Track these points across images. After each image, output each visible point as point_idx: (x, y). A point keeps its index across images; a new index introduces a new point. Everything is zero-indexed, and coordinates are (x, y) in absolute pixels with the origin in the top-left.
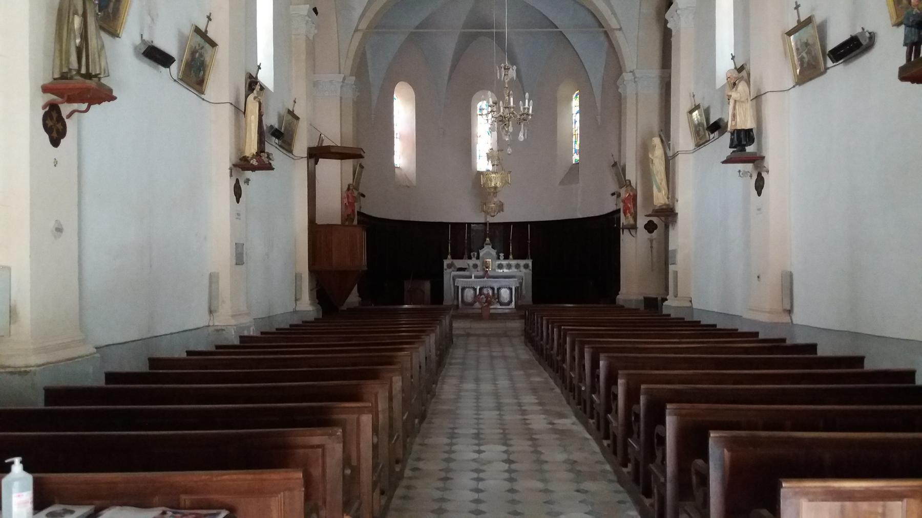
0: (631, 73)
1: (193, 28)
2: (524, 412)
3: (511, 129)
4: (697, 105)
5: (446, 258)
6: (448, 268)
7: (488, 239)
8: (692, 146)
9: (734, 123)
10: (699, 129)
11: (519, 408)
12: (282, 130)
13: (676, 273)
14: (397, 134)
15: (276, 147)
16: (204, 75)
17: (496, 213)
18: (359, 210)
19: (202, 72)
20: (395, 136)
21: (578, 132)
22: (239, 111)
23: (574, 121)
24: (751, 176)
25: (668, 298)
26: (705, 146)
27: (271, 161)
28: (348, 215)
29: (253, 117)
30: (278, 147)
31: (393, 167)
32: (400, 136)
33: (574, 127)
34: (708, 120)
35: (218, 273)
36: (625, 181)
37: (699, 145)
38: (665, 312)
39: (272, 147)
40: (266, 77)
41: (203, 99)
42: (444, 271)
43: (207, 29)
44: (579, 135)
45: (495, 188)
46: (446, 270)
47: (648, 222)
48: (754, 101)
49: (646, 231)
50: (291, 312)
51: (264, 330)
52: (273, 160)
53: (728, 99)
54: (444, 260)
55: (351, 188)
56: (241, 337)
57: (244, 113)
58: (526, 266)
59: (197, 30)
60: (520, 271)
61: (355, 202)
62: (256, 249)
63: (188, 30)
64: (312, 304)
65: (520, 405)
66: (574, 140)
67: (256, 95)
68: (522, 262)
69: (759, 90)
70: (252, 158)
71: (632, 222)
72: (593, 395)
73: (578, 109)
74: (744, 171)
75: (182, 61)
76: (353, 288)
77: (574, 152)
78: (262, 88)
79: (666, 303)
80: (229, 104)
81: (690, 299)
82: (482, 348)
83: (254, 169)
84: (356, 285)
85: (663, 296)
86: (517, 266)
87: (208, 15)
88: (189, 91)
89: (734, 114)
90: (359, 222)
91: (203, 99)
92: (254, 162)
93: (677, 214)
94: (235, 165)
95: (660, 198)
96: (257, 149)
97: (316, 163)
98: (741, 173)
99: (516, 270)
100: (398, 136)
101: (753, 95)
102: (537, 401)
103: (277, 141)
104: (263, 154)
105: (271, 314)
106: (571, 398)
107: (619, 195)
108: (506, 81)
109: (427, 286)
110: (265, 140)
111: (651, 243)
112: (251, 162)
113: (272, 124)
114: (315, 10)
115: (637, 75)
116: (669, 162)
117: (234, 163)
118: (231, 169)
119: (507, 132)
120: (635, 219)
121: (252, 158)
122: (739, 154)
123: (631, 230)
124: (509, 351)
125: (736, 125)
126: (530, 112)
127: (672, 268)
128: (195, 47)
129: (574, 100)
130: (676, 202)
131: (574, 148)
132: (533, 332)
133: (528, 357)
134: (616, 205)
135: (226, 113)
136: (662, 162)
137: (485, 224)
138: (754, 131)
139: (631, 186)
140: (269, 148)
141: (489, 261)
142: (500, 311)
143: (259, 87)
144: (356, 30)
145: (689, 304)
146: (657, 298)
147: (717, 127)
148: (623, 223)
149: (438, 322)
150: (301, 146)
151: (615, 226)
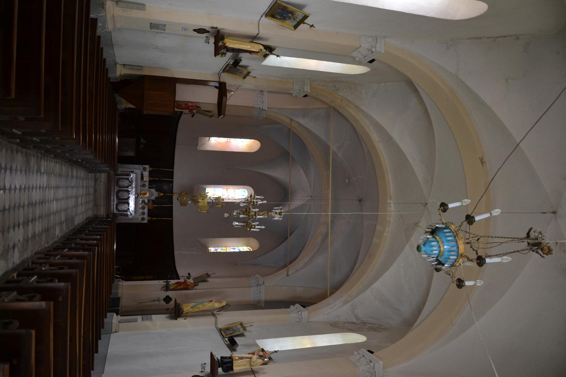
0: (262, 283)
1: (308, 15)
2: (26, 223)
3: (241, 216)
4: (246, 328)
5: (150, 167)
6: (143, 168)
7: (162, 194)
8: (220, 326)
9: (237, 358)
10: (231, 330)
11: (30, 219)
12: (238, 67)
13: (136, 321)
14: (230, 140)
15: (227, 62)
16: (277, 18)
17: (180, 201)
18: (184, 112)
19: (279, 17)
20: (229, 139)
21: (228, 251)
22: (253, 39)
23: (234, 248)
24: (202, 372)
25: (119, 316)
26: (220, 335)
27: (220, 55)
28: (180, 105)
29: (249, 47)
30: (227, 63)
32: (229, 142)
33: (231, 248)
34: (237, 336)
35: (145, 10)
36: (198, 282)
37: (220, 330)
38: (109, 314)
39: (227, 58)
40: (272, 60)
41: (262, 16)
43: (305, 24)
44: (226, 251)
45: (198, 202)
46: (142, 166)
47: (171, 298)
48: (251, 370)
49: (165, 297)
50: (115, 60)
51: (102, 39)
52: (221, 56)
53: (252, 353)
54: (149, 165)
55: (199, 109)
56: (96, 19)
57: (252, 42)
59: (306, 17)
60: (140, 215)
61: (189, 110)
62: (162, 40)
63: (306, 11)
64: (121, 76)
65: (33, 220)
66: (223, 248)
67: (263, 51)
68: (146, 216)
69: (257, 372)
70: (223, 43)
71: (171, 288)
72: (60, 256)
73: (242, 250)
74: (205, 367)
75: (288, 4)
76: (132, 104)
77: (216, 248)
78: (266, 56)
79: (115, 314)
80: (258, 33)
81: (117, 332)
82: (85, 190)
83: (216, 43)
84: (135, 107)
85: (120, 311)
86: (143, 213)
87: (314, 26)
88: (268, 6)
89: (244, 358)
90: (177, 112)
91: (262, 16)
92: (220, 44)
93: (176, 319)
94: (218, 31)
95: (187, 308)
96: (229, 46)
97: (216, 87)
98: (204, 365)
99: (141, 212)
100: (228, 140)
101: (254, 368)
102: (37, 233)
103: (231, 63)
104: (226, 51)
105: (114, 46)
106: (40, 256)
107: (189, 278)
108: (272, 213)
109: (132, 154)
110: (234, 53)
111: (156, 300)
112: (221, 42)
113: (227, 83)
114: (306, 96)
115: (261, 287)
116: (212, 313)
117: (220, 31)
118: (216, 28)
119: (240, 214)
120: (172, 290)
121: (223, 43)
122: (217, 364)
123: (166, 287)
124: (81, 209)
125: (236, 360)
126: (252, 230)
127: (139, 318)
128: (296, 15)
129: (247, 247)
130: (184, 318)
131: (219, 248)
132: (96, 224)
133: (76, 223)
134: (182, 276)
135: (252, 30)
136: (210, 308)
137: (172, 193)
138: (232, 372)
139: (194, 286)
140: (229, 54)
141: (147, 195)
142: (112, 203)
143: (268, 53)
144: (291, 120)
145: (113, 331)
146: (119, 307)
147: (232, 345)
148: (170, 282)
149: (103, 161)
150: (227, 78)
151: (169, 276)
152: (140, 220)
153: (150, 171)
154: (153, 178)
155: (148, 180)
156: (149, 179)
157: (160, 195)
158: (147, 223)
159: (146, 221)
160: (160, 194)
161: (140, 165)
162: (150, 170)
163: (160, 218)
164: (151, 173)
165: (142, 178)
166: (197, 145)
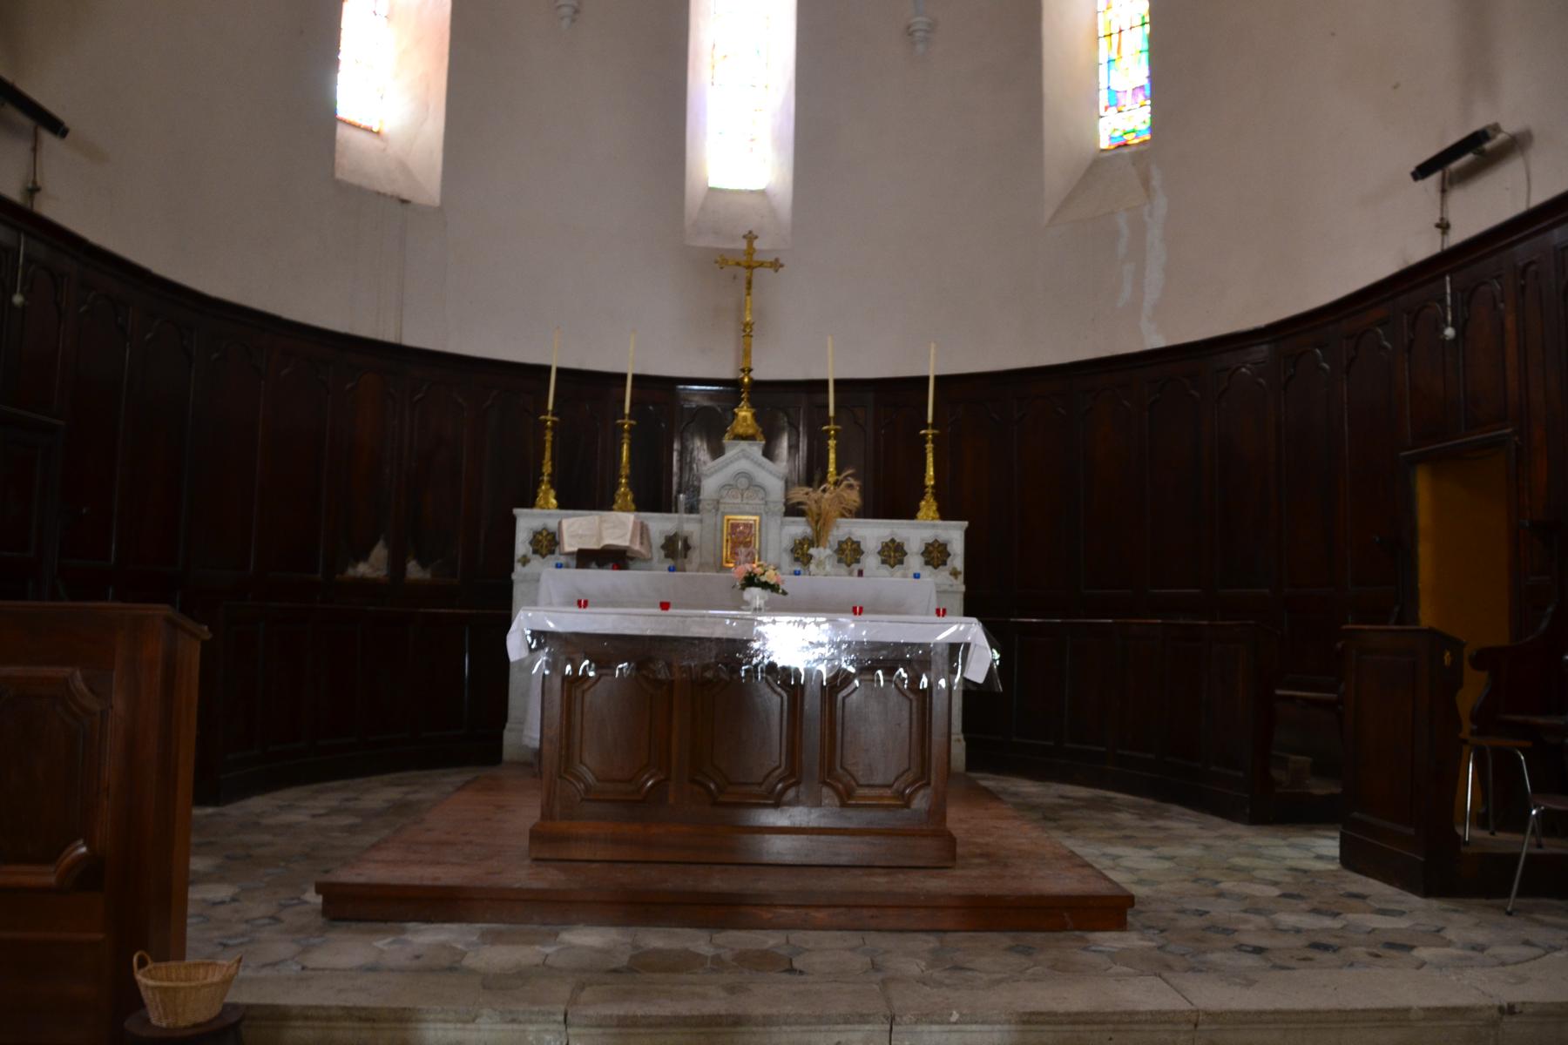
5: (530, 503)
6: (535, 552)
31: (323, 119)
42: (518, 567)
46: (525, 561)
58: (935, 554)
66: (1103, 59)
68: (917, 532)
77: (1103, 102)
131: (1103, 85)
152: (943, 575)
153: (569, 501)
154: (617, 485)
155: (629, 518)
156: (624, 509)
157: (751, 431)
158: (965, 524)
159: (954, 534)
160: (740, 430)
161: (514, 576)
162: (554, 501)
163: (929, 433)
164: (575, 498)
165: (614, 558)
166: (404, 202)
